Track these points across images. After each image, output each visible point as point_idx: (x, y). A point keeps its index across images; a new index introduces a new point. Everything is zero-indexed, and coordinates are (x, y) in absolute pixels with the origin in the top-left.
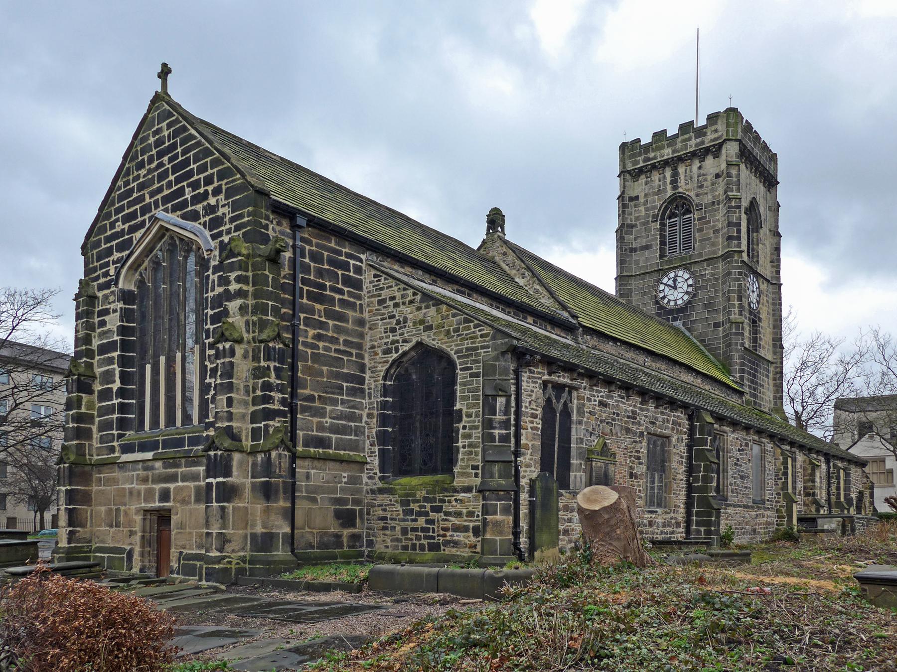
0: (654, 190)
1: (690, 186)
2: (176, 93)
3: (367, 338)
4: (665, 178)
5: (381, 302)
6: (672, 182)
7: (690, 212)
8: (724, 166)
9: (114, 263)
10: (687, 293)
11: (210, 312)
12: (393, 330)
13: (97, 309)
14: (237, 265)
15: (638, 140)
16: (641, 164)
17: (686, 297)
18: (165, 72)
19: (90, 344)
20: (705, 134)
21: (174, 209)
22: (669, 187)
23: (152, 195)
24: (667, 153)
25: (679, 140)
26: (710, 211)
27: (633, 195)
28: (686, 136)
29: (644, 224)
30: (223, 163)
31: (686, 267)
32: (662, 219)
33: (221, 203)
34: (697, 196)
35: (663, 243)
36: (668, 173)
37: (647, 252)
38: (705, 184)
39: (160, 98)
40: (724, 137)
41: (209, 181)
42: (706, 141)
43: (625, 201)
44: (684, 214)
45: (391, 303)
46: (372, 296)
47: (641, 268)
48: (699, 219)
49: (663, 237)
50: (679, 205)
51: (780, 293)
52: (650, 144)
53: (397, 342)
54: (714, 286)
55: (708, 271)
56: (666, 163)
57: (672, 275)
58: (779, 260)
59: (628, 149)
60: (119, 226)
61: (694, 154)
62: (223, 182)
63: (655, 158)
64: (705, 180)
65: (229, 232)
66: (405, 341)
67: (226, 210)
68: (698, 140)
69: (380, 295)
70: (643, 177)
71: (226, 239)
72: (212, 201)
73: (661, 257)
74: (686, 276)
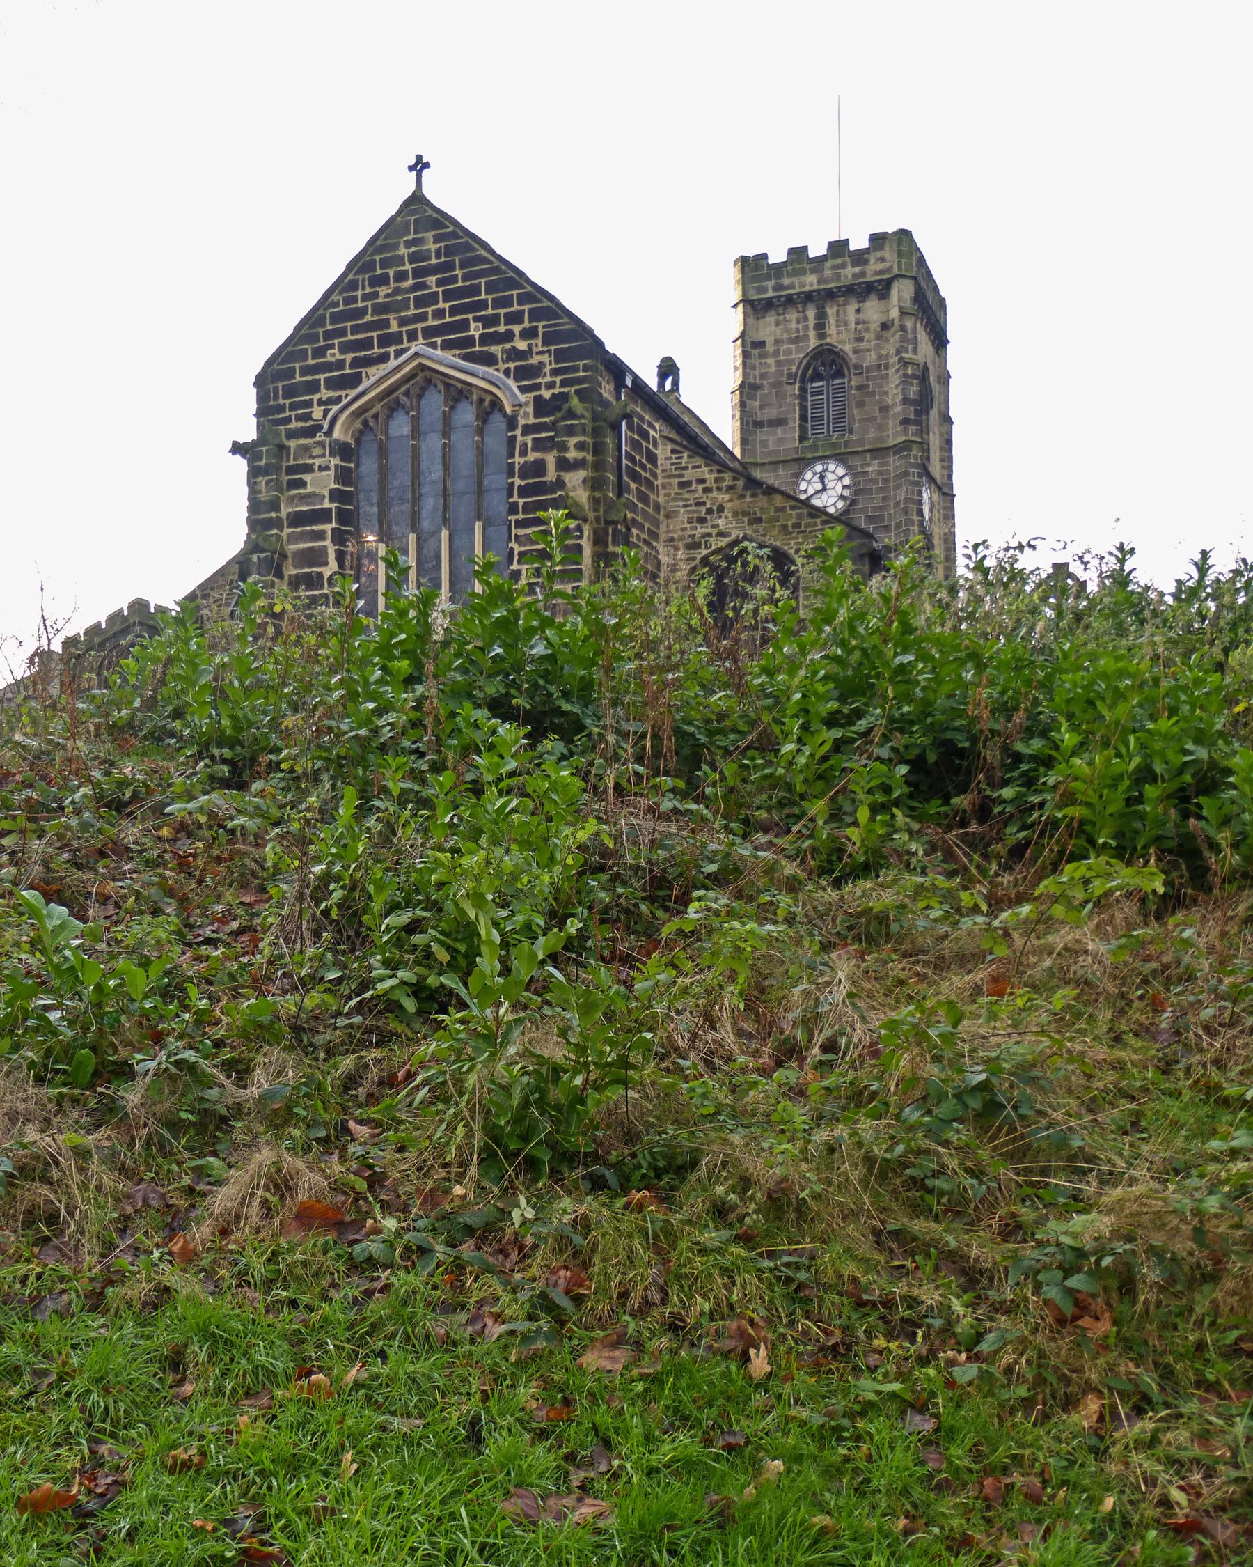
0: (793, 334)
1: (844, 336)
2: (429, 192)
3: (663, 528)
4: (806, 319)
5: (683, 485)
6: (817, 327)
7: (843, 376)
8: (894, 313)
9: (320, 403)
10: (842, 497)
11: (518, 482)
12: (702, 520)
13: (285, 464)
14: (579, 429)
15: (764, 256)
16: (770, 294)
17: (840, 504)
18: (419, 166)
19: (278, 509)
20: (866, 262)
21: (447, 346)
22: (812, 333)
23: (403, 322)
24: (810, 282)
25: (828, 264)
26: (875, 378)
27: (759, 338)
28: (839, 261)
29: (774, 385)
30: (539, 301)
31: (841, 458)
32: (803, 380)
33: (535, 350)
34: (855, 352)
35: (803, 418)
36: (811, 313)
37: (779, 431)
38: (867, 336)
39: (417, 201)
40: (896, 271)
41: (515, 318)
42: (869, 273)
43: (751, 347)
44: (834, 376)
45: (700, 487)
46: (670, 477)
47: (770, 452)
48: (859, 388)
49: (803, 409)
50: (827, 363)
51: (952, 509)
52: (784, 264)
53: (709, 535)
54: (881, 490)
55: (873, 467)
56: (808, 297)
57: (819, 468)
58: (950, 459)
59: (752, 268)
60: (334, 355)
61: (849, 291)
62: (541, 325)
63: (791, 287)
64: (867, 330)
65: (551, 386)
66: (721, 534)
67: (545, 358)
68: (857, 270)
69: (681, 476)
70: (772, 313)
71: (547, 394)
72: (522, 345)
73: (802, 438)
74: (841, 471)
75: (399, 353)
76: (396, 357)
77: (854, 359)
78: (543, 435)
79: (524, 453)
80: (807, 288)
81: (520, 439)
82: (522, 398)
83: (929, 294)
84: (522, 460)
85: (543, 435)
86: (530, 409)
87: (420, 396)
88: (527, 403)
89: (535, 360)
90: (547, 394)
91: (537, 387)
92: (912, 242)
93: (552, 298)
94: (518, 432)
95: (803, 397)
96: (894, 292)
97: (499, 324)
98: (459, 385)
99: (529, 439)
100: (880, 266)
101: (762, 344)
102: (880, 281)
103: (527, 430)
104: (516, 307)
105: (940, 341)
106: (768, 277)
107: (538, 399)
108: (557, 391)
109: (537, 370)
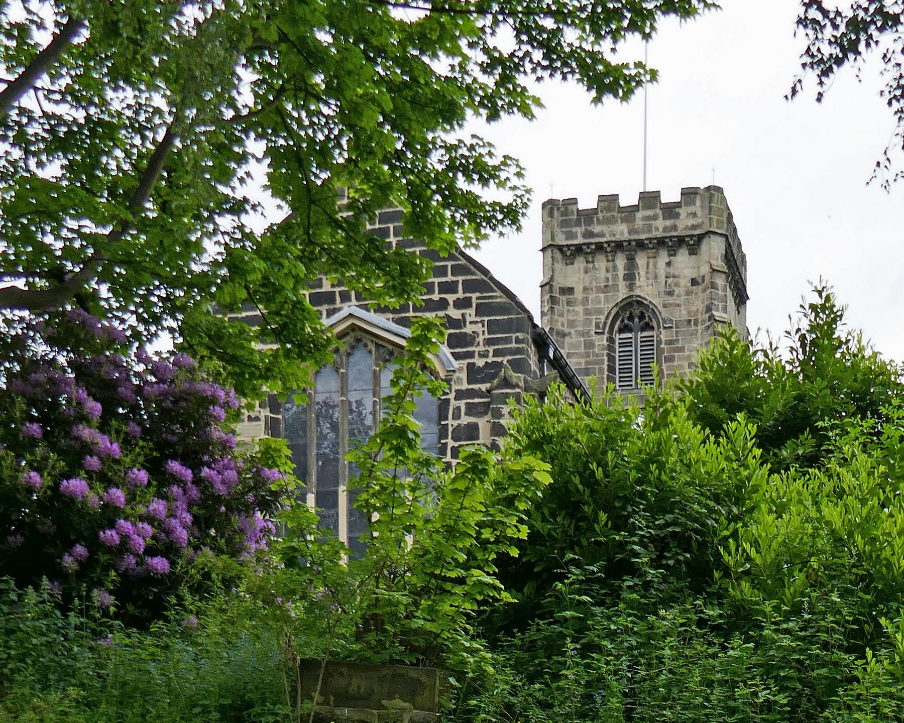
4: (615, 268)
7: (652, 328)
8: (705, 270)
15: (574, 201)
16: (580, 240)
24: (621, 231)
25: (639, 215)
28: (650, 213)
30: (473, 274)
33: (468, 319)
36: (621, 262)
38: (677, 291)
40: (706, 228)
41: (449, 288)
49: (611, 359)
52: (595, 211)
56: (619, 246)
61: (661, 243)
63: (602, 235)
65: (484, 355)
67: (478, 328)
68: (668, 223)
71: (480, 362)
72: (455, 314)
75: (330, 313)
76: (328, 316)
77: (665, 313)
78: (477, 400)
79: (457, 416)
80: (618, 237)
81: (453, 403)
82: (456, 364)
83: (735, 251)
84: (456, 423)
85: (477, 400)
86: (464, 375)
87: (349, 355)
88: (461, 369)
89: (468, 329)
90: (480, 362)
91: (471, 355)
92: (724, 200)
93: (485, 272)
94: (452, 396)
95: (611, 348)
96: (704, 246)
97: (433, 292)
98: (390, 347)
99: (462, 404)
100: (691, 222)
101: (570, 290)
102: (691, 236)
103: (460, 395)
104: (450, 278)
105: (741, 297)
106: (578, 223)
107: (471, 366)
108: (490, 360)
109: (469, 340)
